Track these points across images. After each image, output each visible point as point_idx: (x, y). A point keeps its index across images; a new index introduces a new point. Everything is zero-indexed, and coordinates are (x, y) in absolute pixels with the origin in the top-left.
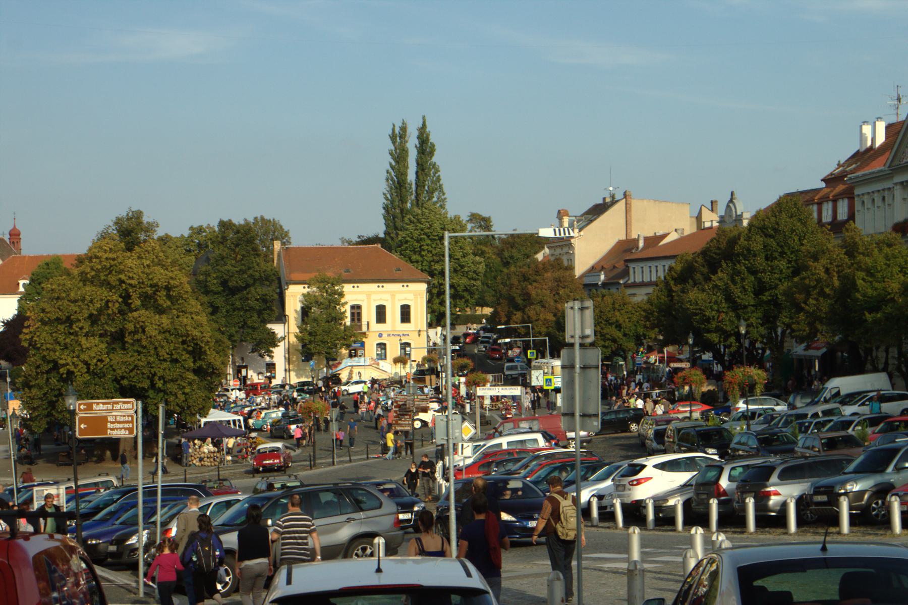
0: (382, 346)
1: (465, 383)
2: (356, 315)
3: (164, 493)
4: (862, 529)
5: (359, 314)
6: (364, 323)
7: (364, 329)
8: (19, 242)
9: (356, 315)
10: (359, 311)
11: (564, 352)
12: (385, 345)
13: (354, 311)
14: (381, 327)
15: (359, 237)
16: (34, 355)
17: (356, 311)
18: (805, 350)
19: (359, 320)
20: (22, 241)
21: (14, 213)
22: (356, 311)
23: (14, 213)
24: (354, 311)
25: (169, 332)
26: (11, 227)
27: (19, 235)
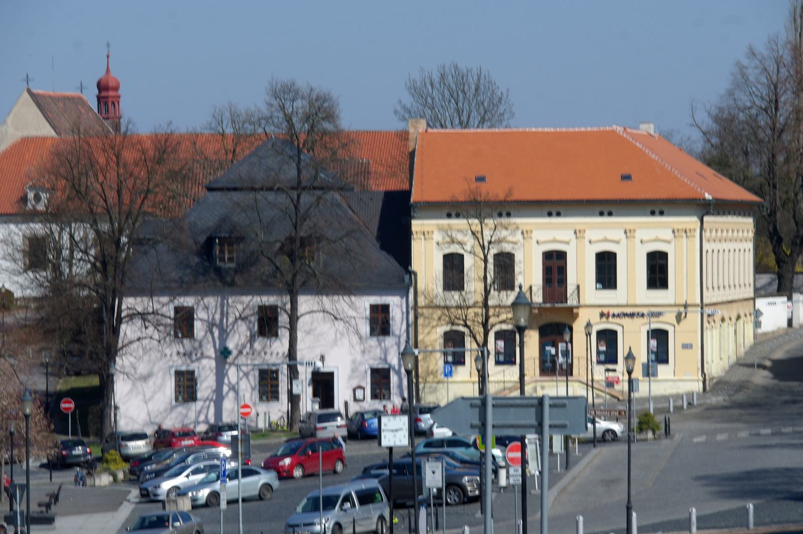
0: (608, 338)
1: (547, 362)
2: (555, 271)
3: (318, 475)
4: (391, 322)
5: (562, 271)
6: (571, 288)
7: (571, 301)
8: (116, 101)
9: (555, 271)
10: (560, 263)
12: (614, 333)
13: (550, 263)
14: (607, 297)
17: (555, 263)
19: (563, 281)
20: (122, 101)
21: (108, 45)
22: (555, 263)
23: (108, 45)
24: (550, 263)
25: (410, 113)
26: (101, 74)
27: (116, 89)
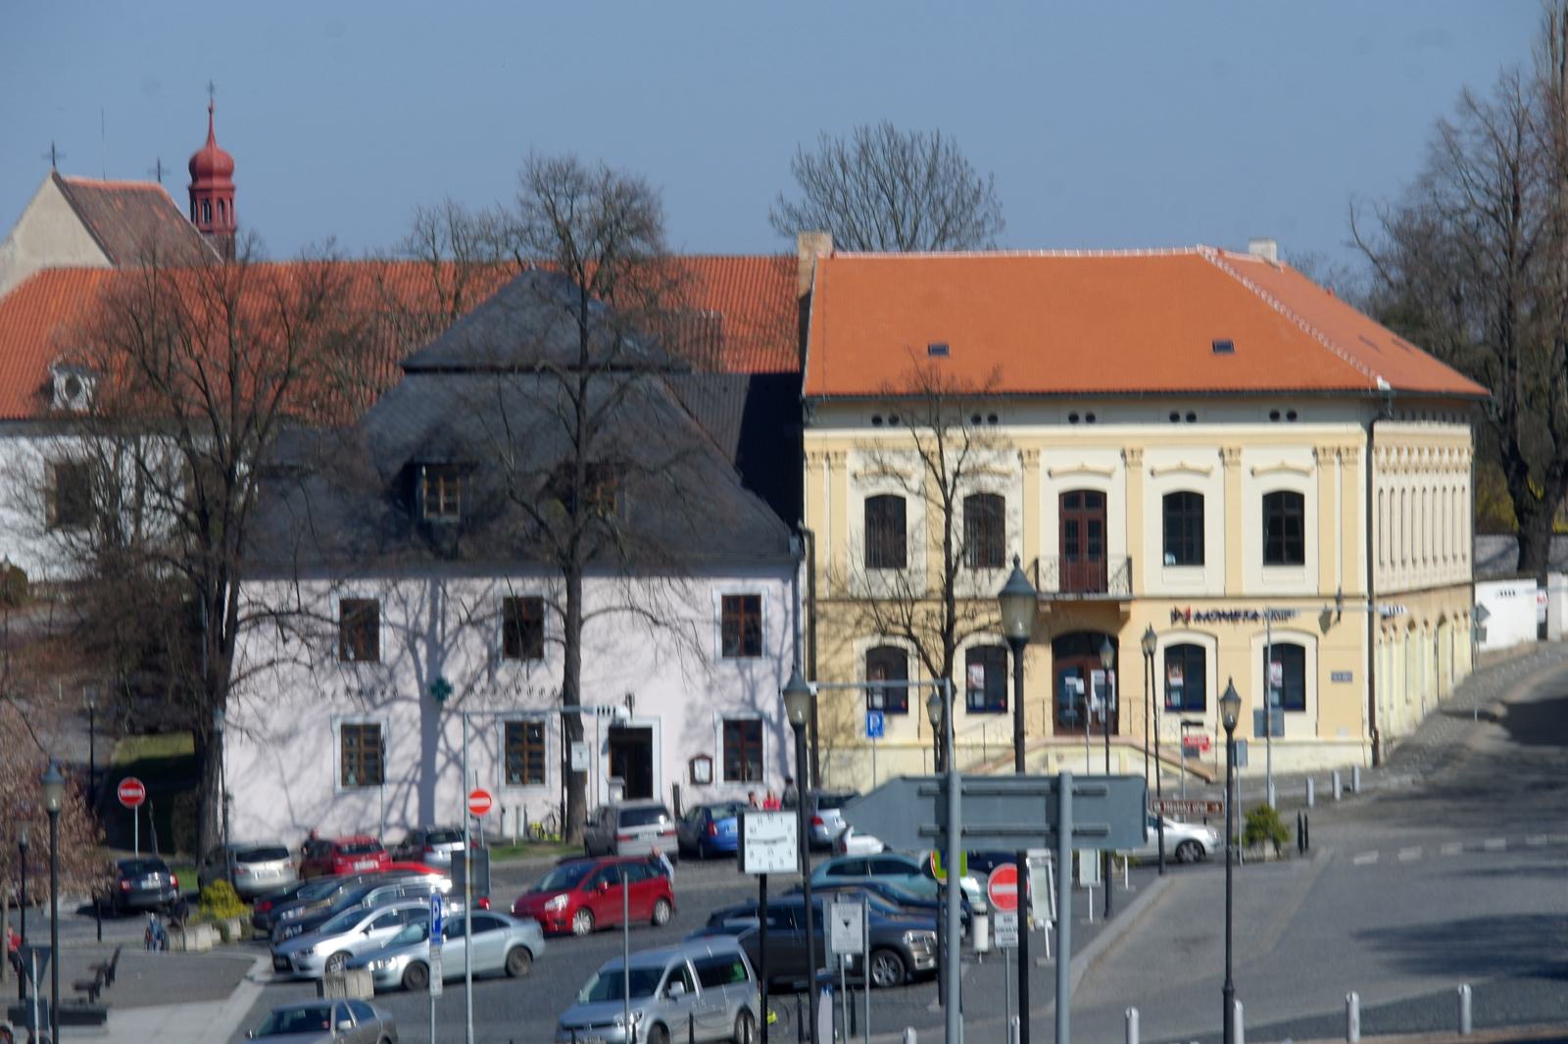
0: (1188, 660)
2: (1084, 531)
5: (1098, 529)
6: (1114, 564)
7: (1116, 589)
8: (226, 198)
9: (1084, 531)
10: (1094, 513)
11: (120, 873)
12: (1199, 651)
13: (1074, 514)
14: (1185, 580)
15: (1001, 204)
16: (365, 591)
17: (1084, 514)
18: (254, 962)
19: (1099, 549)
20: (238, 197)
21: (211, 89)
22: (1084, 514)
23: (211, 89)
24: (1074, 514)
26: (198, 144)
27: (227, 173)
